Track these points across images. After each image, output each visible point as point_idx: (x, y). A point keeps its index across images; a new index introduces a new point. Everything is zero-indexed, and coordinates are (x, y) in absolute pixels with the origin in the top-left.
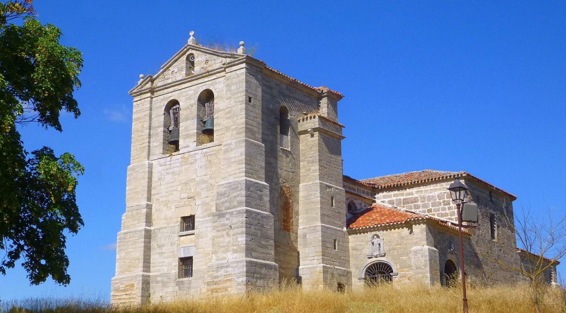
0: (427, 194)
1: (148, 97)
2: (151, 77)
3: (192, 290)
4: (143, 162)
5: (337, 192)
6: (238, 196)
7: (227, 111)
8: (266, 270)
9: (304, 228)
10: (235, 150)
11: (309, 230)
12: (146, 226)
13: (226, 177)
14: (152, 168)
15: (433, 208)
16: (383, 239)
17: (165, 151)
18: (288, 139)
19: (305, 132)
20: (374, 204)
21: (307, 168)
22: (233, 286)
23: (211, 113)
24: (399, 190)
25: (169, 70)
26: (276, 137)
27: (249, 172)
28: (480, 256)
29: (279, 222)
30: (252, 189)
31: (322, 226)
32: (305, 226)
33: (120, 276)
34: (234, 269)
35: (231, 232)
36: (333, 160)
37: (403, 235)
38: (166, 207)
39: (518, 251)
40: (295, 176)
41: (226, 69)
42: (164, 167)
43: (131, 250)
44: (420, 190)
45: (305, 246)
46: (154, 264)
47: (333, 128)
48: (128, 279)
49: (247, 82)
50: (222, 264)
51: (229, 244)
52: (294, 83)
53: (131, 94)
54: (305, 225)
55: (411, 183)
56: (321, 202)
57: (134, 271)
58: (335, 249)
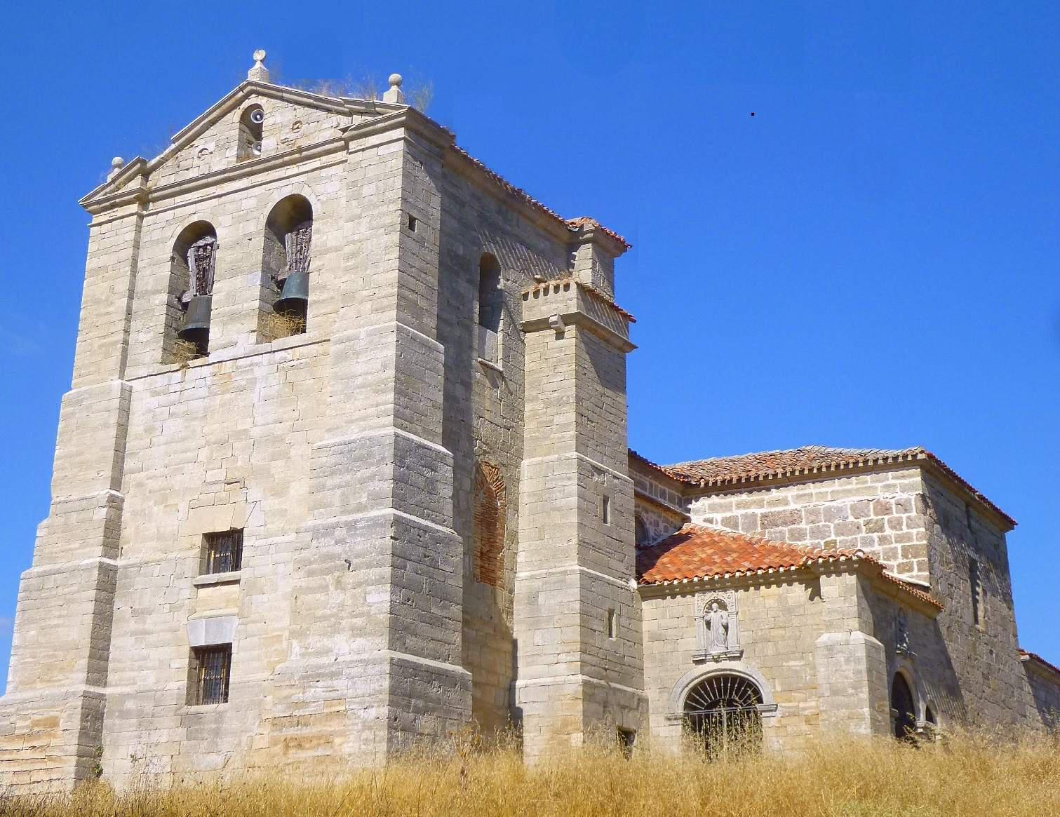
0: (823, 503)
2: (144, 162)
3: (225, 739)
5: (616, 486)
6: (372, 478)
7: (347, 250)
8: (440, 687)
9: (532, 578)
11: (546, 583)
15: (838, 539)
16: (737, 613)
17: (169, 354)
18: (496, 340)
19: (542, 325)
20: (686, 528)
21: (544, 418)
22: (349, 731)
23: (301, 259)
24: (751, 492)
25: (192, 146)
26: (469, 330)
27: (403, 414)
28: (955, 664)
29: (469, 558)
30: (410, 461)
31: (582, 573)
32: (533, 573)
33: (20, 696)
34: (354, 683)
35: (350, 578)
36: (608, 401)
37: (791, 602)
39: (1023, 658)
41: (350, 143)
42: (163, 399)
43: (55, 622)
44: (807, 491)
45: (535, 623)
47: (610, 320)
49: (406, 175)
51: (342, 610)
53: (86, 206)
55: (784, 474)
57: (61, 680)
58: (610, 635)
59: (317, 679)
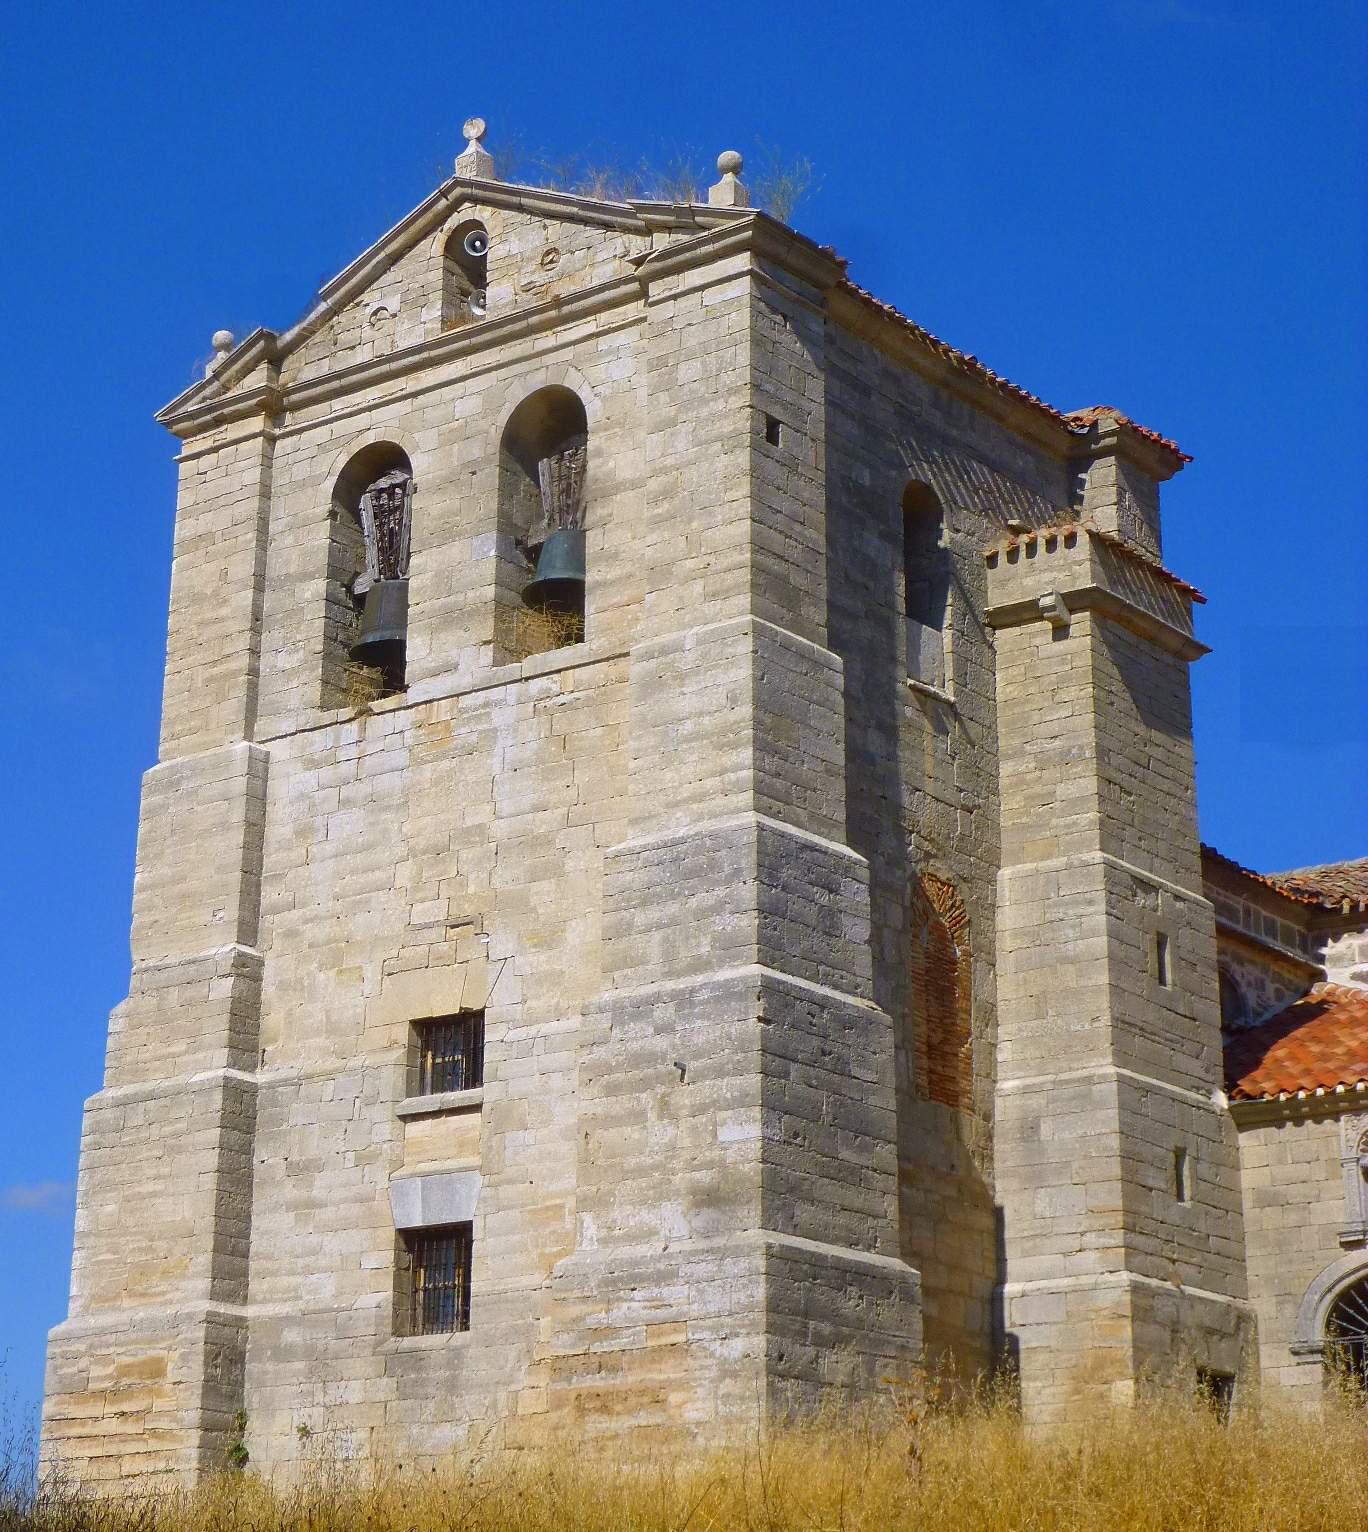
1: (254, 436)
2: (271, 338)
4: (218, 750)
6: (718, 908)
7: (653, 485)
8: (861, 1297)
9: (1026, 1091)
10: (698, 678)
11: (1054, 1100)
12: (228, 1066)
13: (654, 816)
14: (266, 781)
17: (333, 692)
18: (941, 643)
19: (1024, 613)
20: (1318, 991)
21: (1038, 789)
22: (695, 1380)
23: (568, 506)
25: (358, 305)
26: (888, 627)
31: (1121, 1079)
33: (92, 1322)
34: (701, 1292)
35: (685, 1097)
36: (1158, 753)
38: (332, 973)
40: (977, 828)
42: (326, 773)
43: (149, 1187)
45: (1035, 1177)
46: (269, 1257)
48: (134, 1336)
49: (758, 341)
50: (635, 1263)
51: (673, 1157)
52: (968, 370)
53: (169, 424)
54: (1033, 1072)
56: (1111, 957)
58: (1180, 1197)
59: (632, 1286)
